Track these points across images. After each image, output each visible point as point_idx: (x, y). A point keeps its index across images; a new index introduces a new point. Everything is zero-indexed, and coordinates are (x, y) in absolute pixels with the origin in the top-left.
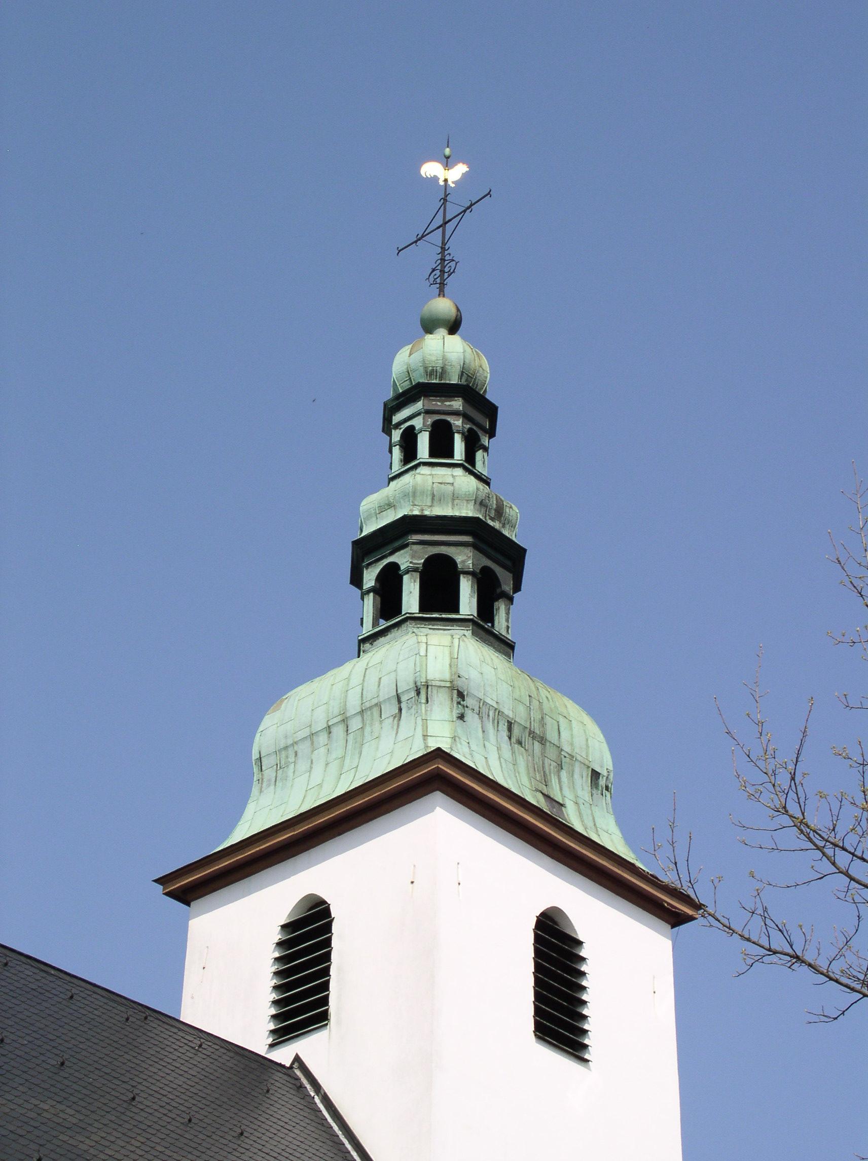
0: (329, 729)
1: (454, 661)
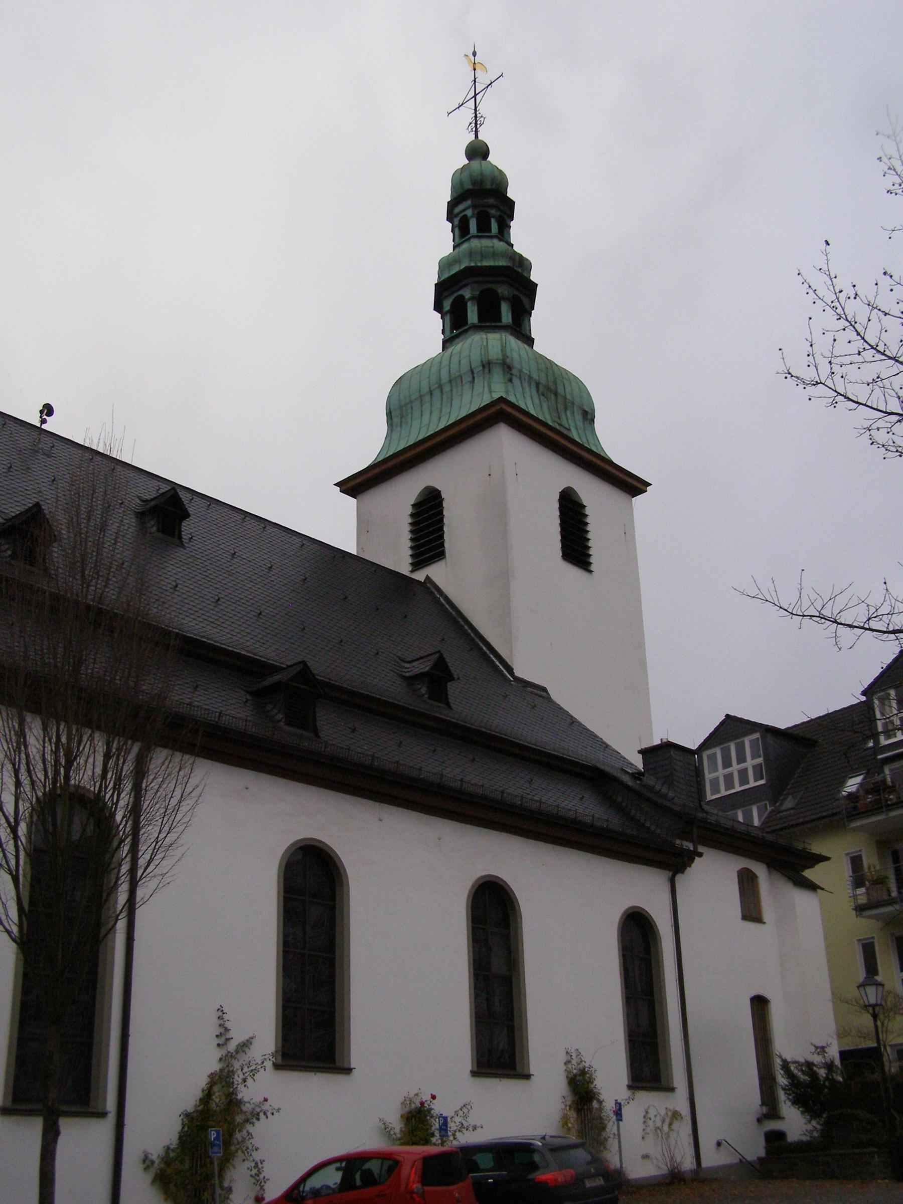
0: (431, 392)
1: (503, 350)
